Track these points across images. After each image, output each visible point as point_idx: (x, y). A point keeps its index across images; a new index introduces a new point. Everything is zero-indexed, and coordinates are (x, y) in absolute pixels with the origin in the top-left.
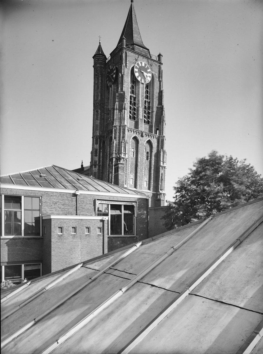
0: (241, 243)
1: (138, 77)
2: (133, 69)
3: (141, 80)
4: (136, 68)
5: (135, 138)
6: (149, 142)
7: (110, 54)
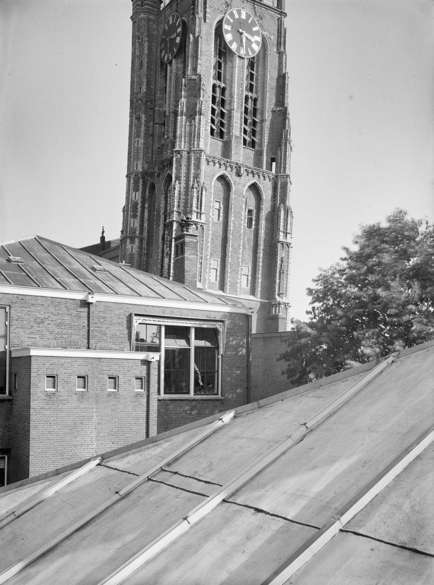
1: (231, 42)
2: (220, 23)
3: (238, 50)
4: (228, 23)
5: (222, 178)
6: (254, 188)
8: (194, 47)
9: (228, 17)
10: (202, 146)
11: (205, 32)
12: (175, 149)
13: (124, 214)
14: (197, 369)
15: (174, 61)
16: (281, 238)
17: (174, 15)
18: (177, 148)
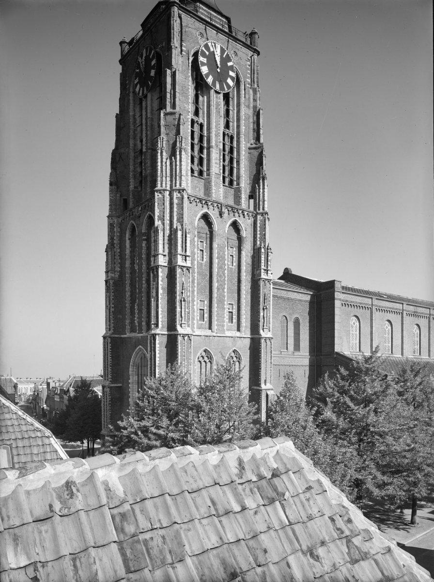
0: (25, 567)
1: (207, 75)
2: (196, 55)
3: (214, 83)
4: (204, 55)
5: (206, 217)
6: (235, 225)
7: (142, 25)
9: (203, 49)
10: (184, 185)
11: (180, 63)
12: (156, 189)
14: (66, 449)
15: (149, 95)
17: (147, 47)
18: (159, 187)
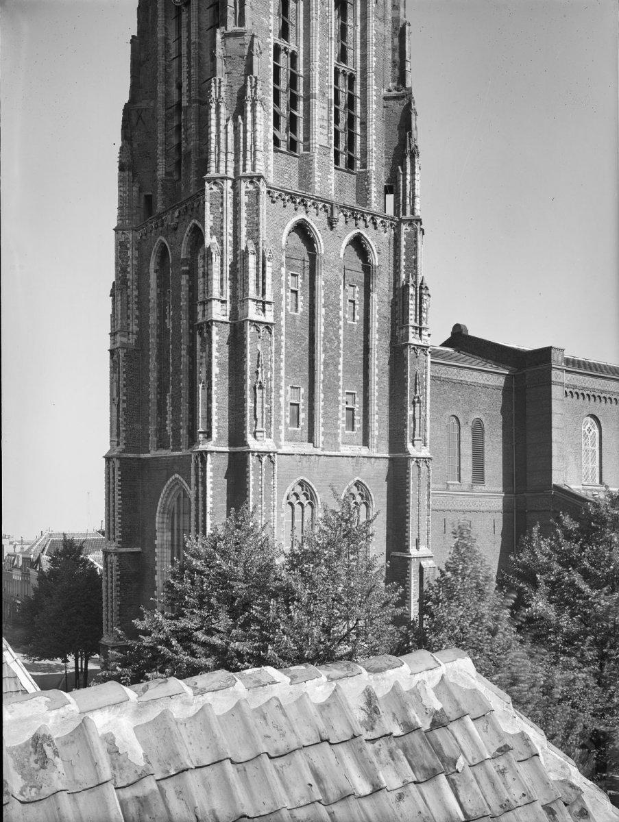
5: (302, 229)
6: (358, 244)
8: (406, 192)
12: (208, 175)
13: (114, 302)
16: (413, 339)
18: (212, 172)
